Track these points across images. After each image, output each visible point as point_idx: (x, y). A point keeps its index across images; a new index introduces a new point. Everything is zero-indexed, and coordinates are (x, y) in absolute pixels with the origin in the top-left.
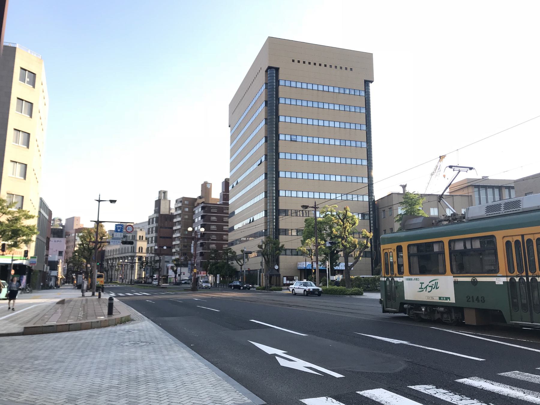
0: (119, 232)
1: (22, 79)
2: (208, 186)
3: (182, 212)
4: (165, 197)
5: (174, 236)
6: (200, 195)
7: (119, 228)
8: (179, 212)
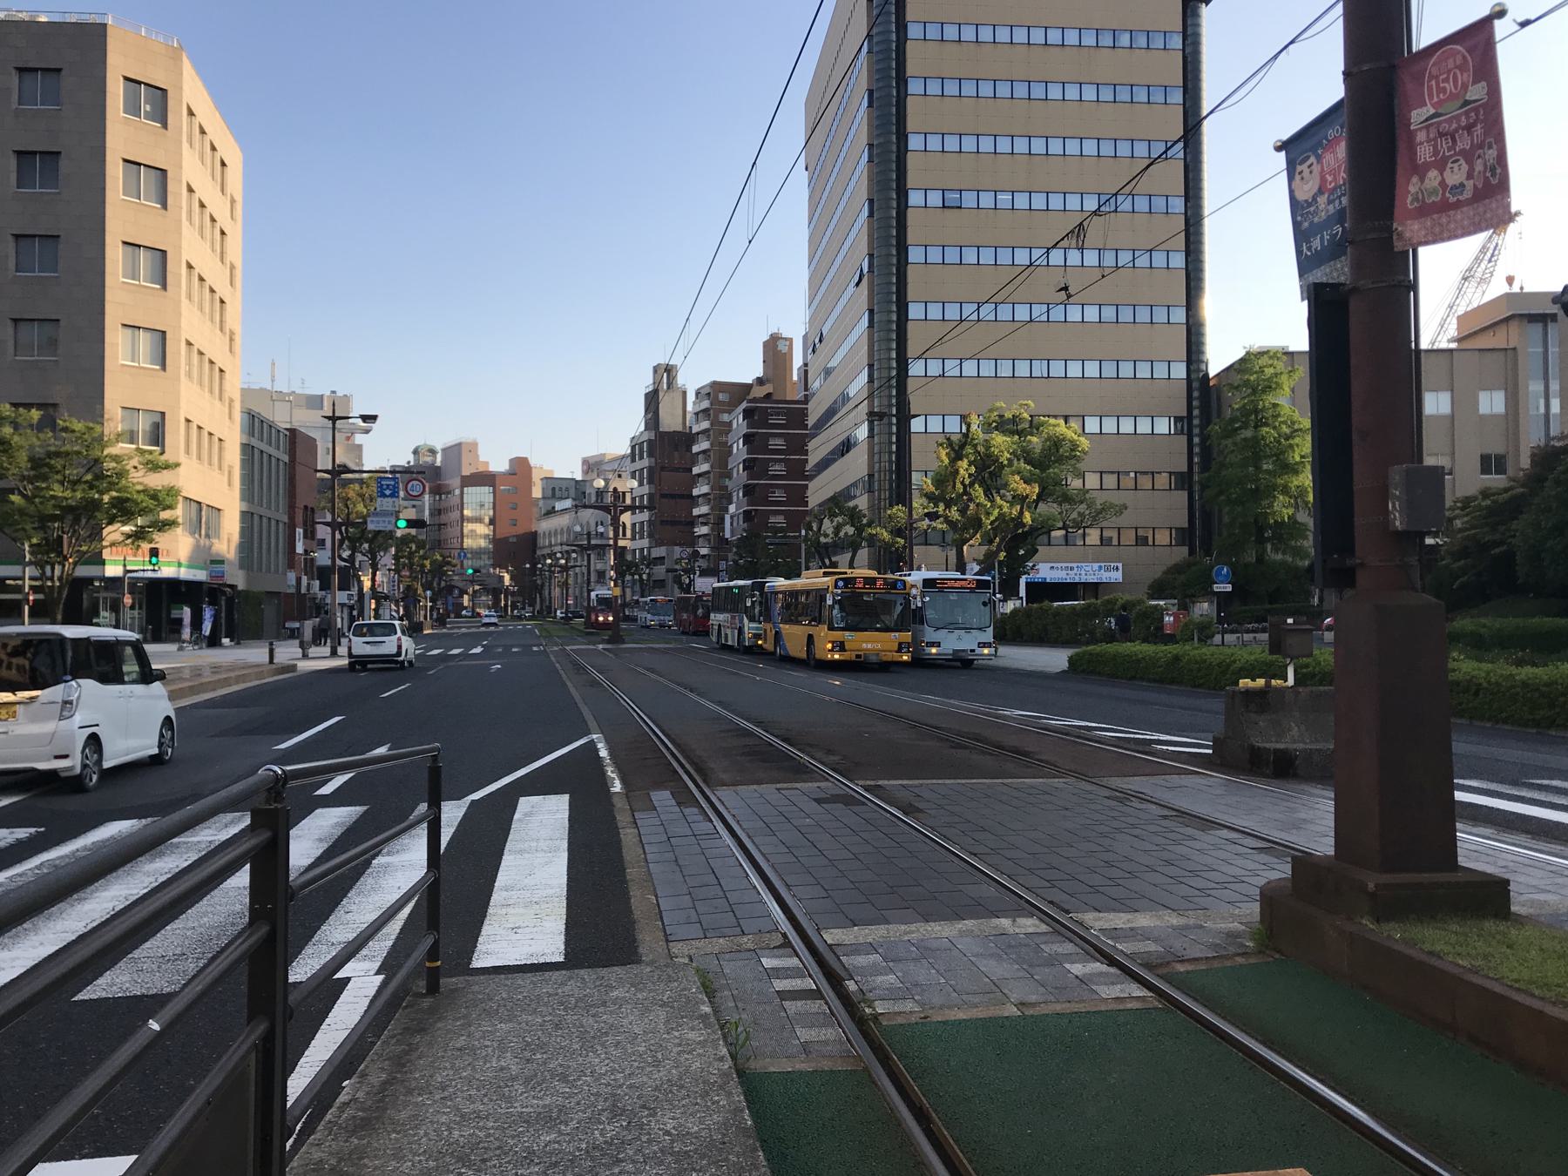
0: (388, 496)
1: (133, 108)
2: (782, 347)
3: (712, 424)
4: (671, 383)
5: (696, 492)
6: (759, 372)
7: (388, 485)
8: (705, 425)
